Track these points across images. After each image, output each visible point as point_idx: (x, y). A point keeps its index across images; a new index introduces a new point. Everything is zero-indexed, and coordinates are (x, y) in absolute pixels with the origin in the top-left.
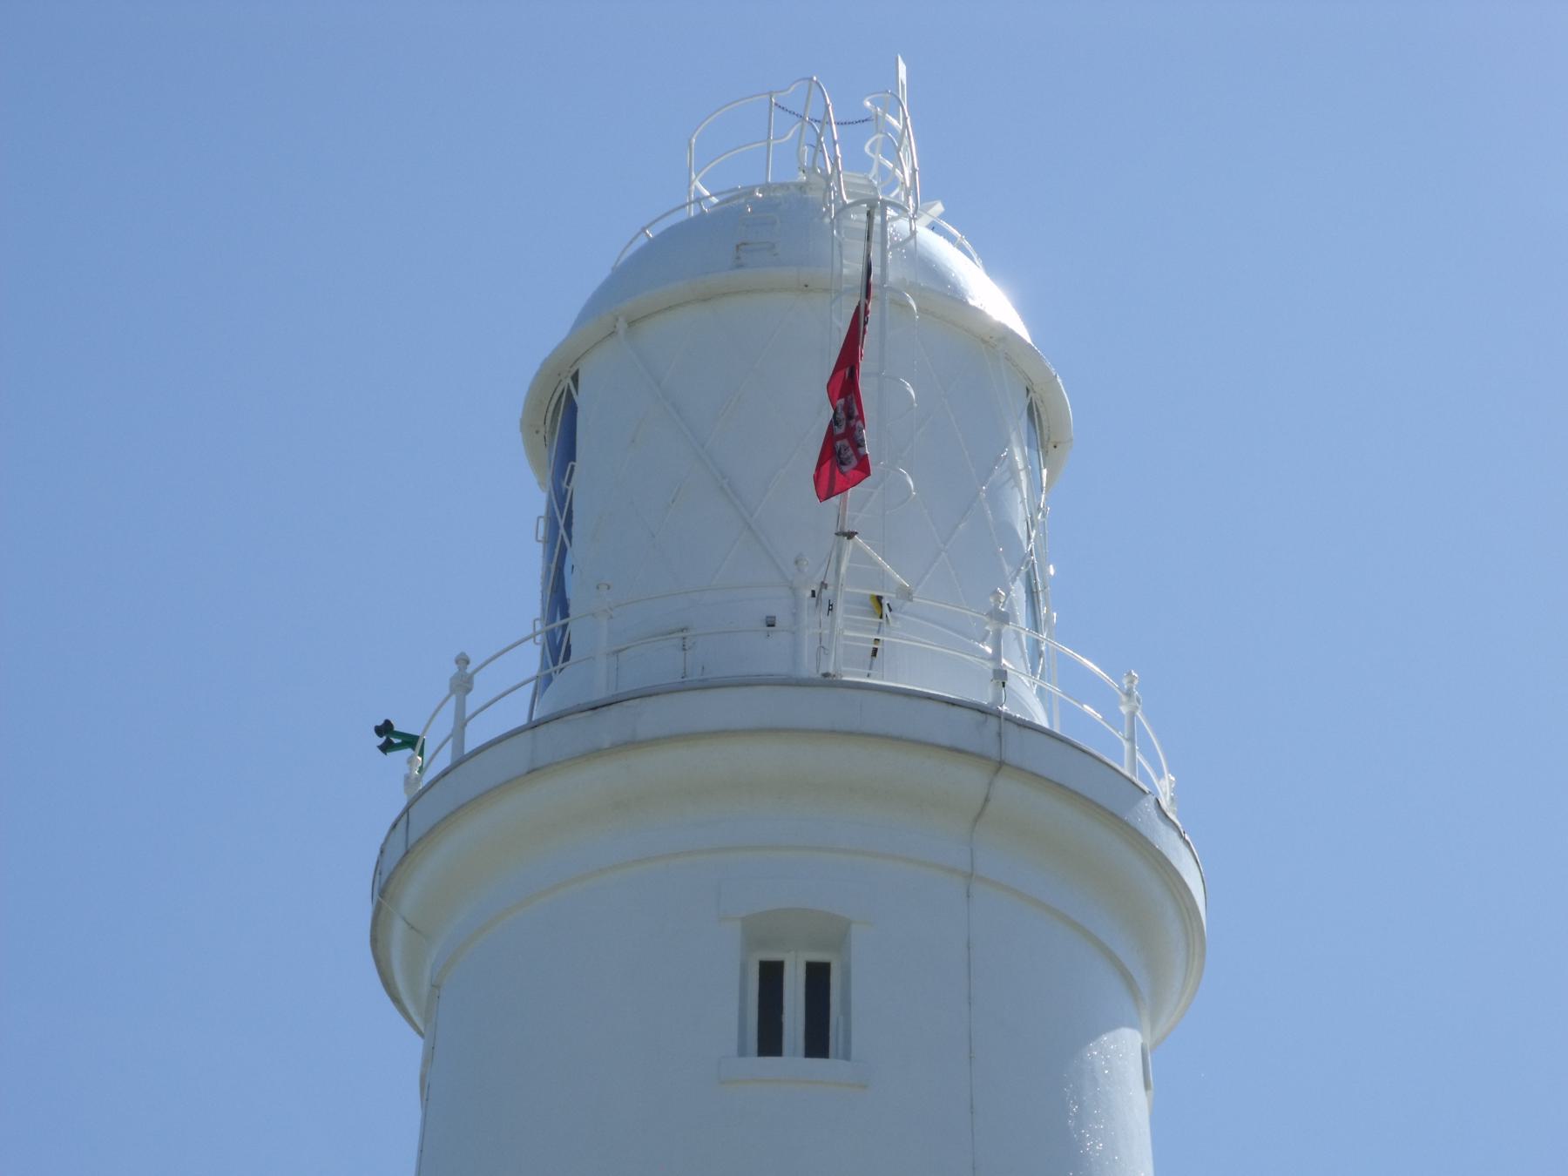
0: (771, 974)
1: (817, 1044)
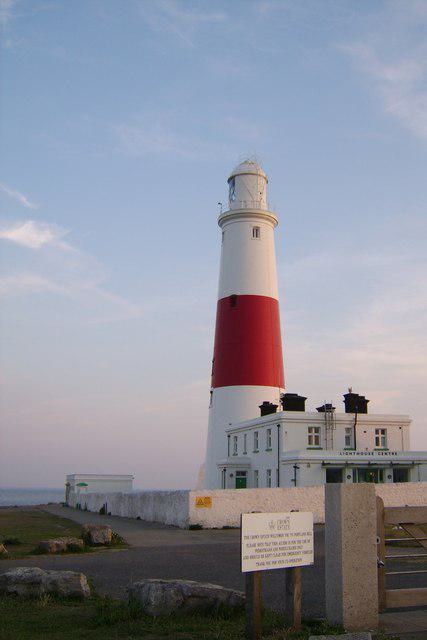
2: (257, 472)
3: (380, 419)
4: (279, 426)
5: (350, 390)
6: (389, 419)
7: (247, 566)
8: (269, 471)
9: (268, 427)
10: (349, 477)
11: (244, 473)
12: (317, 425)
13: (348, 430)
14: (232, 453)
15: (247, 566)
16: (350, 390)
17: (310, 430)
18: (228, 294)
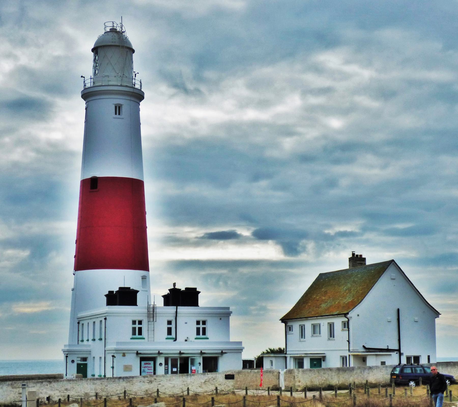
0: (119, 114)
1: (119, 114)
2: (94, 357)
3: (20, 377)
4: (105, 319)
5: (174, 284)
6: (15, 378)
7: (347, 267)
8: (101, 358)
9: (94, 320)
10: (161, 364)
11: (85, 359)
12: (140, 319)
13: (169, 323)
14: (80, 339)
15: (347, 267)
16: (174, 284)
17: (198, 323)
18: (89, 176)
